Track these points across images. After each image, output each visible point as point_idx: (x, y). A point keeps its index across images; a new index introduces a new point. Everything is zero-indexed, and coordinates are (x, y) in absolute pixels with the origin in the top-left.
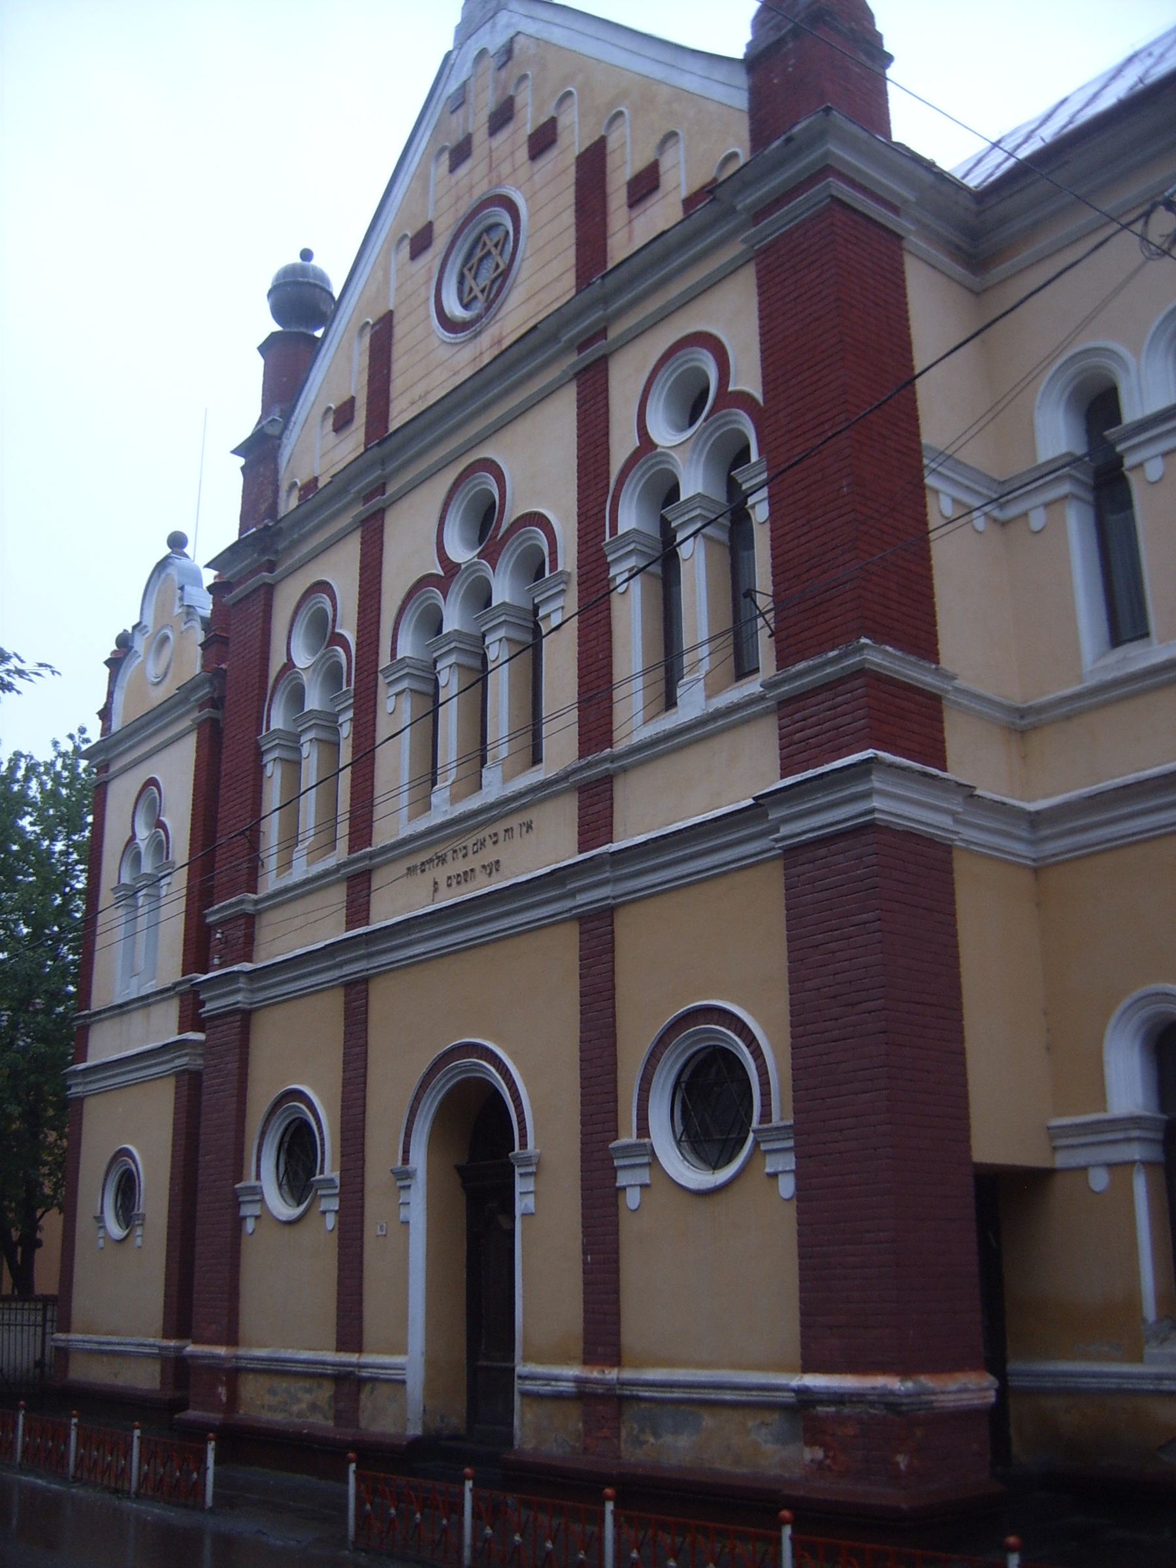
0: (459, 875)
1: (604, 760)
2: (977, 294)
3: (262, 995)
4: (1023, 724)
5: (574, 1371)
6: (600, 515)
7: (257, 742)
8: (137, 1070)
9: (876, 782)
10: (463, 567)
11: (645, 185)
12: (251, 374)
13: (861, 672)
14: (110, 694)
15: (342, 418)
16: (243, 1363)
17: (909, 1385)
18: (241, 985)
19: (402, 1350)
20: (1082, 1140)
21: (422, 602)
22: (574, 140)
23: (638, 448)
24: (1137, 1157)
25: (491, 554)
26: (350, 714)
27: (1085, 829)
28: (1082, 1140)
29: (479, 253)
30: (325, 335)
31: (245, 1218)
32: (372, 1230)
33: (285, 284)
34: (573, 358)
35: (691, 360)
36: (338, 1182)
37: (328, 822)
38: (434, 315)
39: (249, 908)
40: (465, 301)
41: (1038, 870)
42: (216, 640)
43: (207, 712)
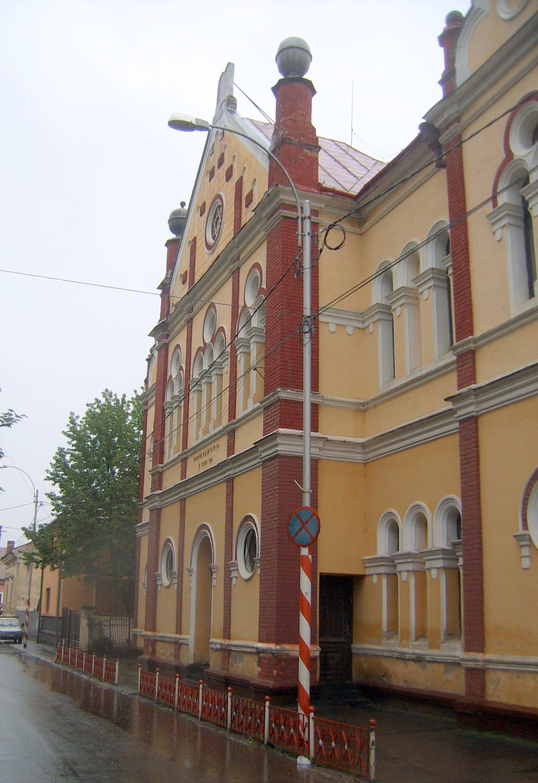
9: (279, 440)
13: (279, 400)
14: (148, 373)
16: (156, 638)
17: (278, 647)
19: (188, 634)
20: (373, 564)
24: (383, 572)
27: (376, 450)
28: (373, 564)
32: (184, 591)
33: (174, 219)
36: (177, 573)
39: (160, 470)
41: (366, 464)
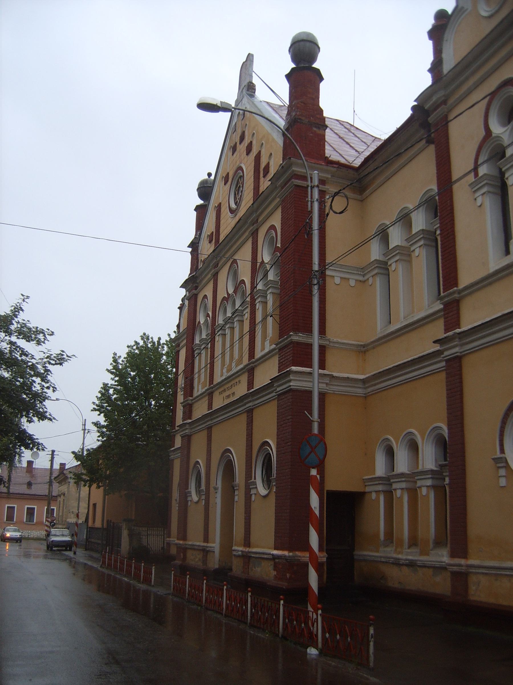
1: (454, 293)
3: (193, 430)
4: (363, 350)
5: (241, 549)
9: (291, 377)
14: (180, 319)
17: (291, 554)
27: (375, 385)
31: (251, 495)
39: (190, 402)
41: (366, 397)
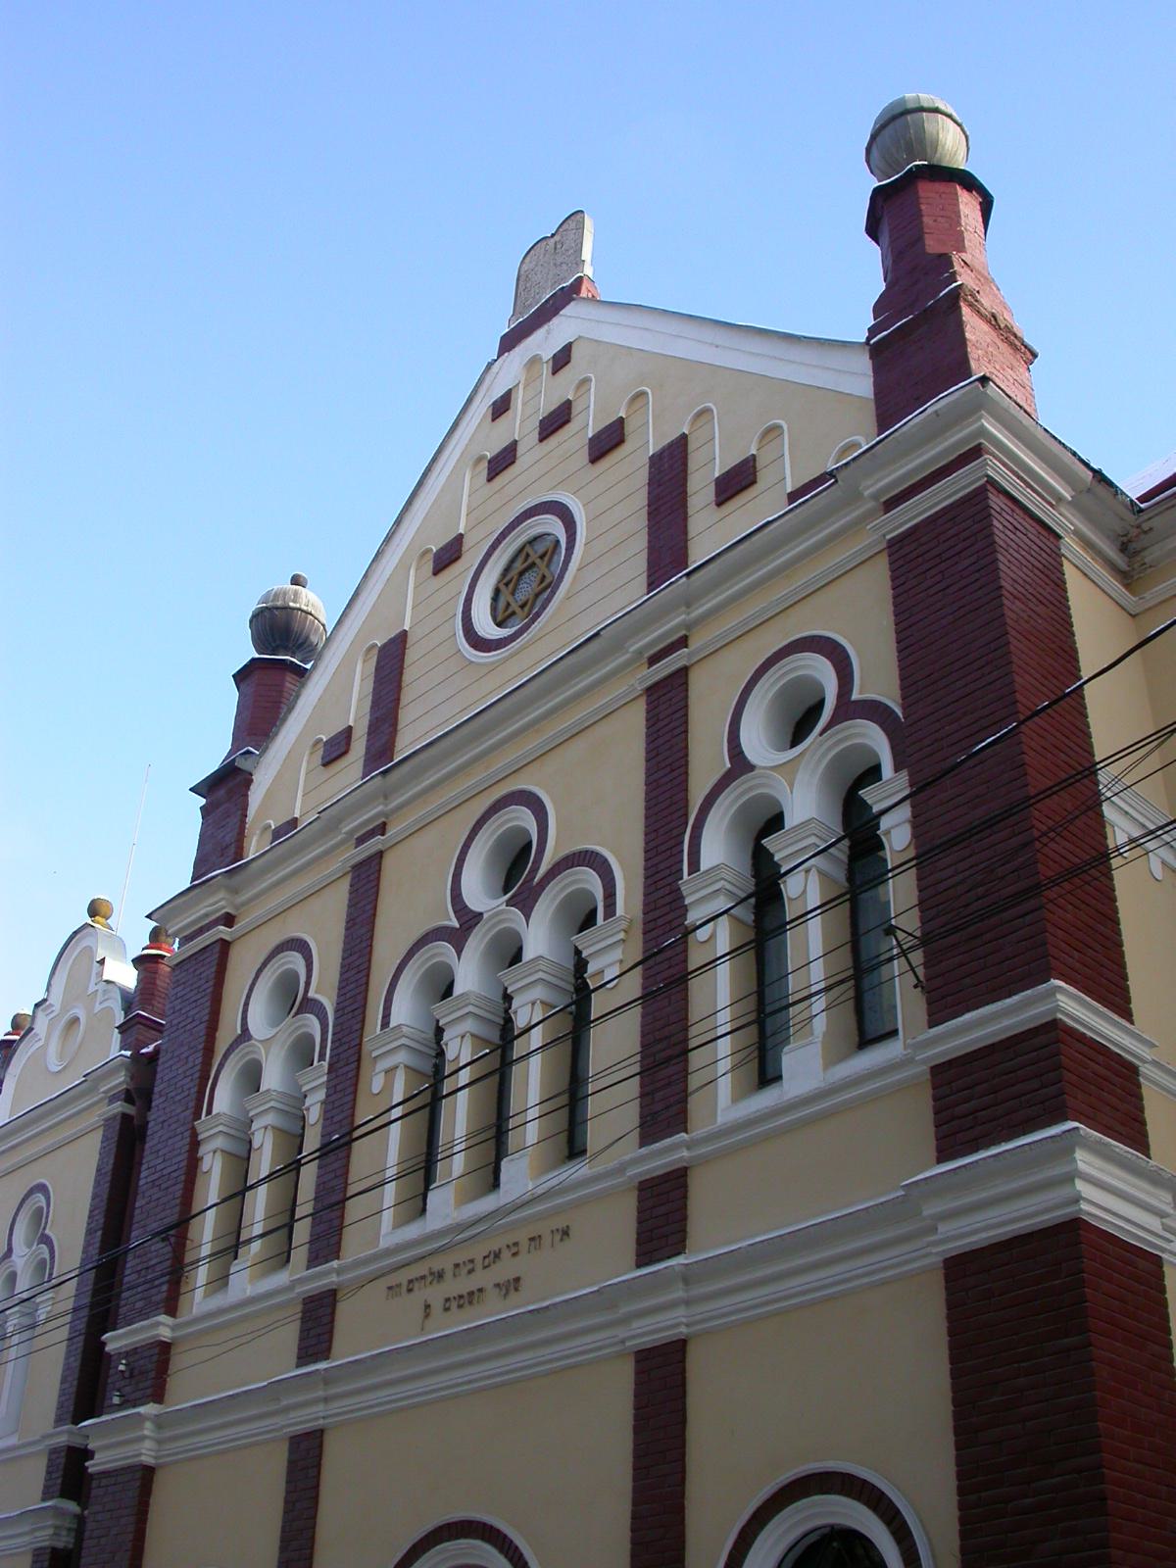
0: (461, 1297)
2: (1133, 616)
6: (674, 851)
7: (193, 1129)
8: (546, 1342)
10: (485, 916)
11: (736, 482)
12: (228, 700)
15: (336, 749)
18: (146, 1432)
21: (428, 959)
22: (648, 439)
23: (730, 770)
25: (525, 902)
26: (321, 1095)
29: (519, 566)
30: (314, 667)
34: (645, 671)
35: (803, 667)
37: (283, 1225)
38: (460, 633)
40: (499, 619)
42: (139, 1016)
43: (119, 1107)
